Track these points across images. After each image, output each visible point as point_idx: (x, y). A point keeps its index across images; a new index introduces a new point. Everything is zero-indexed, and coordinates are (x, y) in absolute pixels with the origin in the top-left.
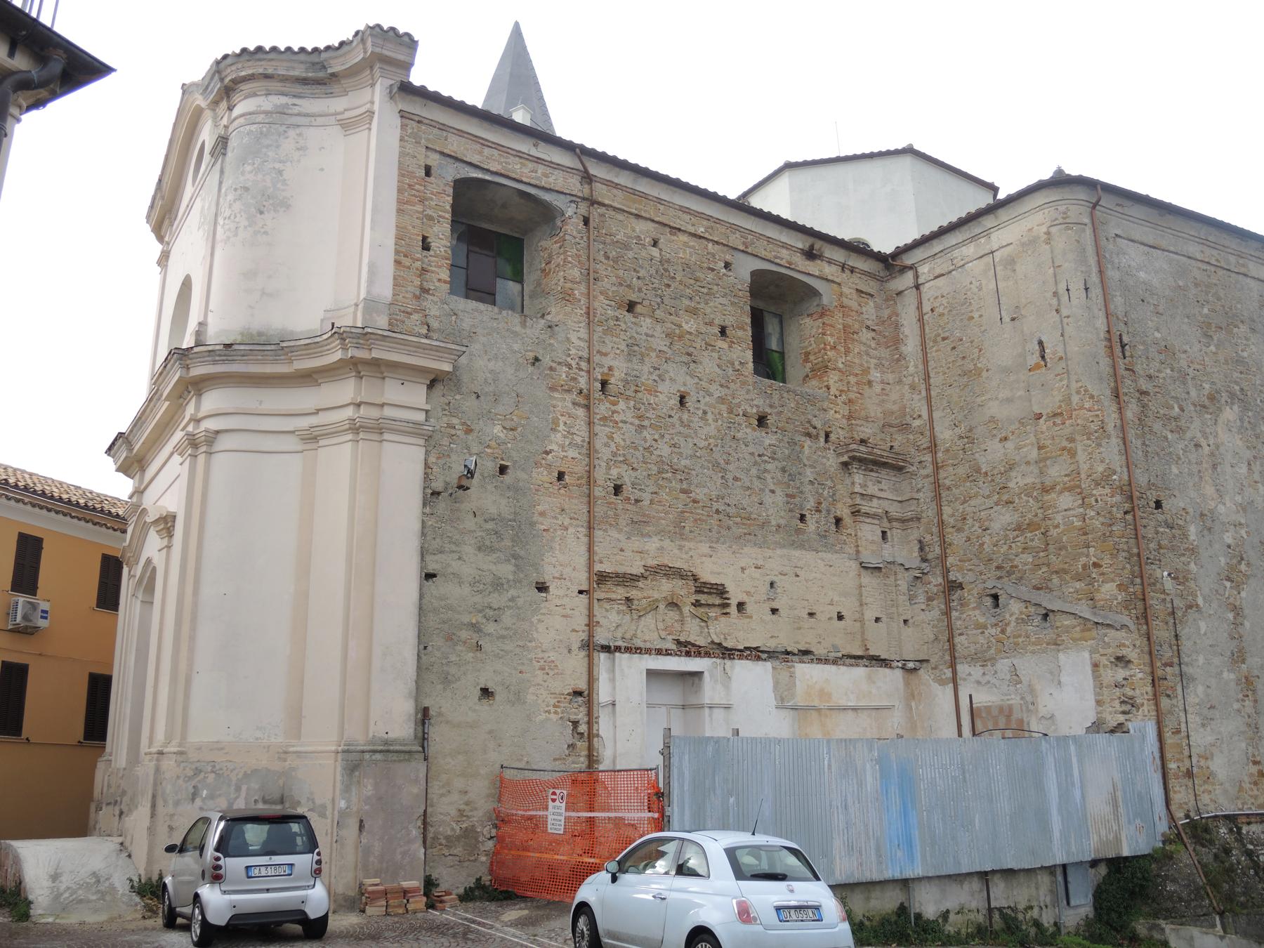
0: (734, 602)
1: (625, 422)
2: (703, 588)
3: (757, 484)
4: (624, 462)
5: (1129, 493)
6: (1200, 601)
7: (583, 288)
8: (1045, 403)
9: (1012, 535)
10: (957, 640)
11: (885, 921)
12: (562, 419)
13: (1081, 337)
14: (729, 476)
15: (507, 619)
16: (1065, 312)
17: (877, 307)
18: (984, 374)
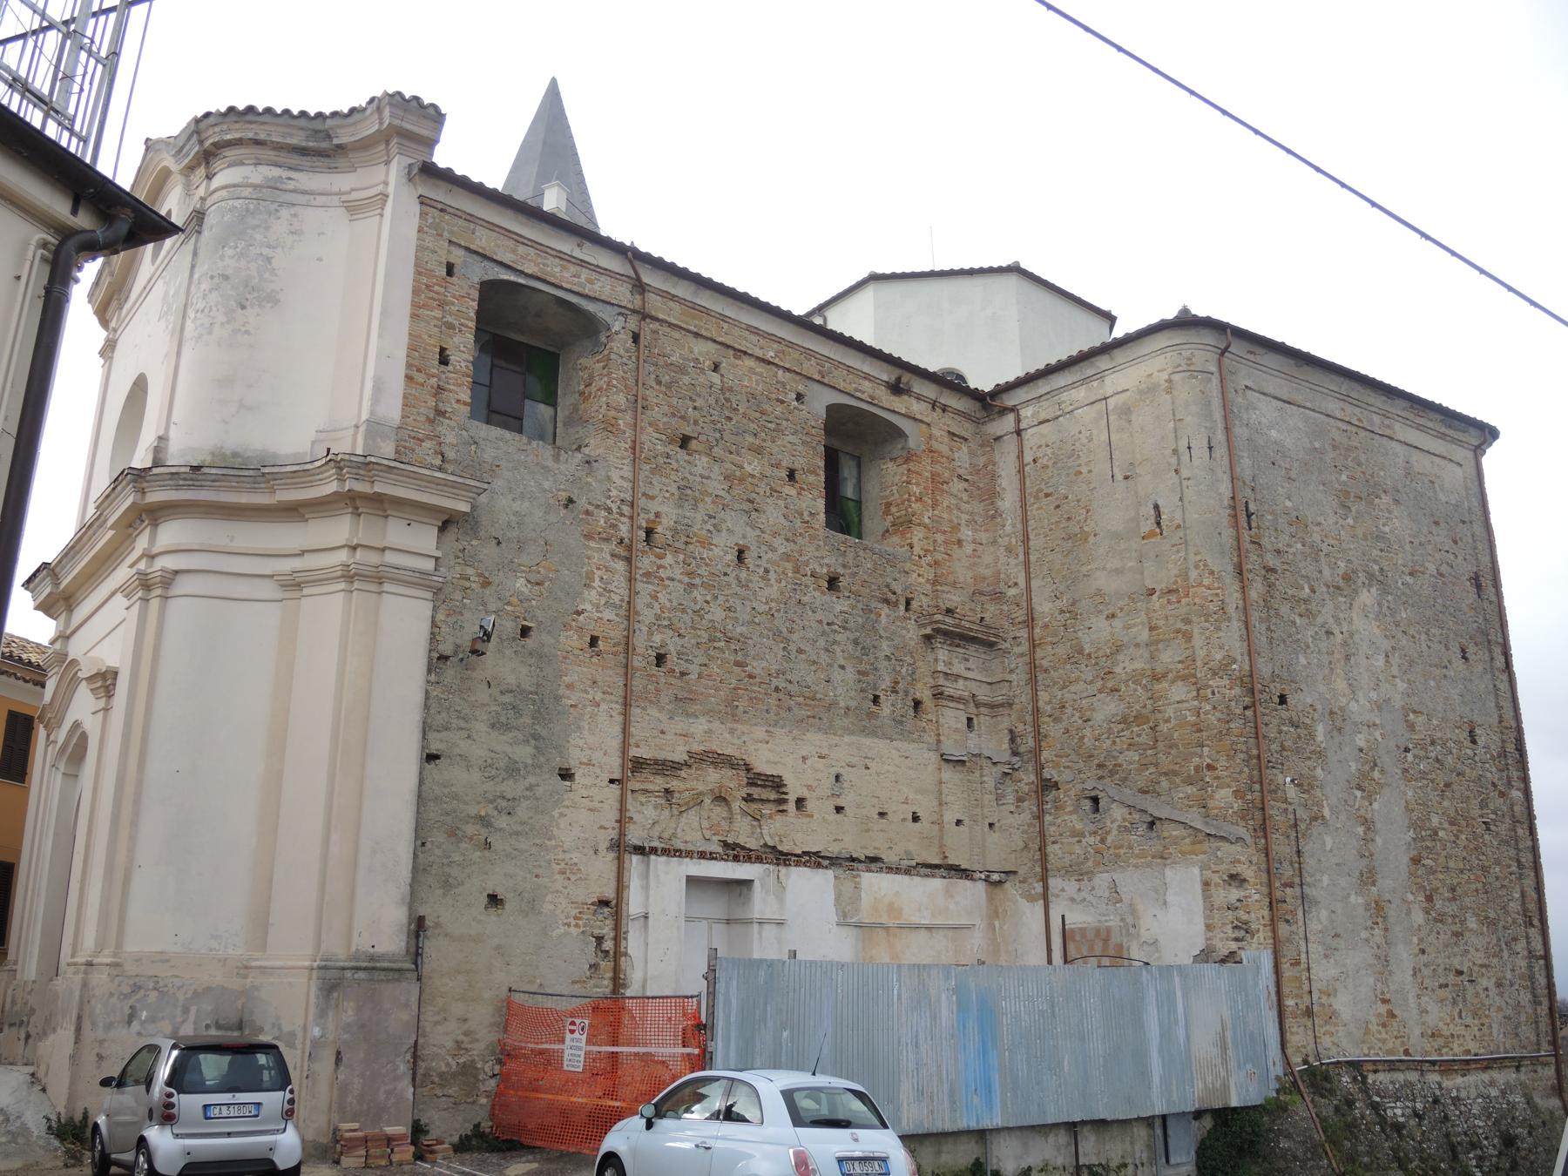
0: (792, 798)
4: (669, 626)
5: (1249, 684)
6: (1326, 812)
7: (629, 417)
8: (1160, 577)
9: (1116, 728)
10: (1050, 849)
14: (792, 647)
15: (523, 811)
16: (1185, 473)
17: (972, 454)
18: (1092, 539)
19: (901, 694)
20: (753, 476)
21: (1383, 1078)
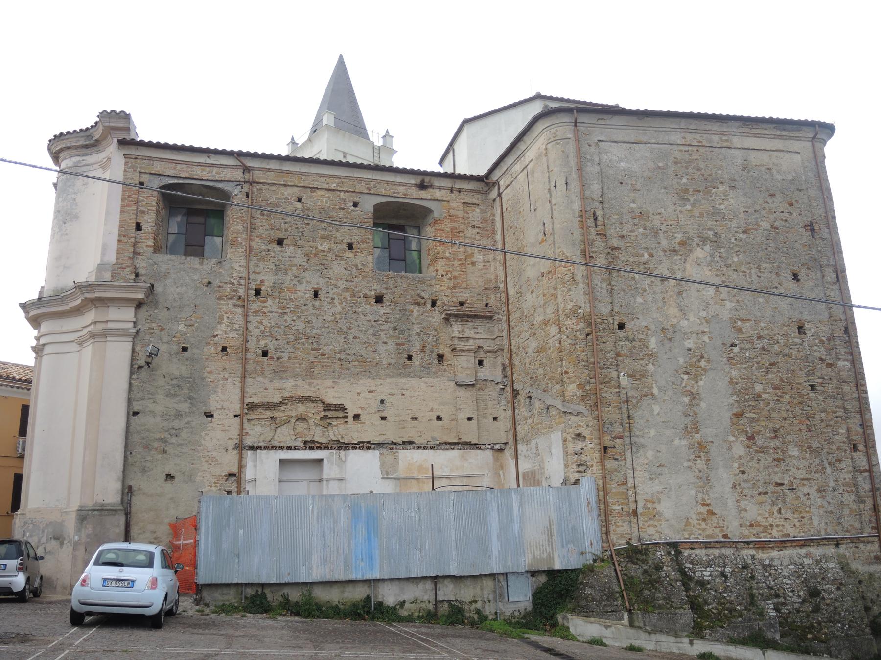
0: (351, 415)
1: (271, 312)
2: (328, 407)
3: (372, 339)
4: (271, 336)
6: (655, 391)
11: (355, 605)
12: (225, 316)
14: (351, 337)
15: (184, 434)
16: (554, 202)
17: (482, 211)
19: (428, 352)
20: (324, 251)
21: (700, 553)
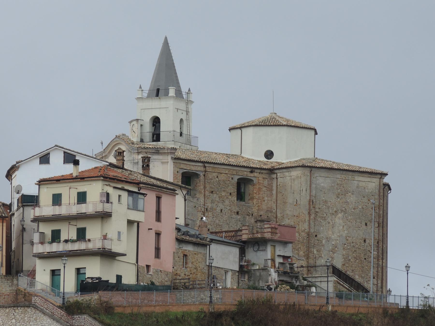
5: (308, 234)
6: (323, 256)
7: (203, 190)
13: (304, 201)
14: (230, 226)
16: (301, 195)
17: (268, 181)
